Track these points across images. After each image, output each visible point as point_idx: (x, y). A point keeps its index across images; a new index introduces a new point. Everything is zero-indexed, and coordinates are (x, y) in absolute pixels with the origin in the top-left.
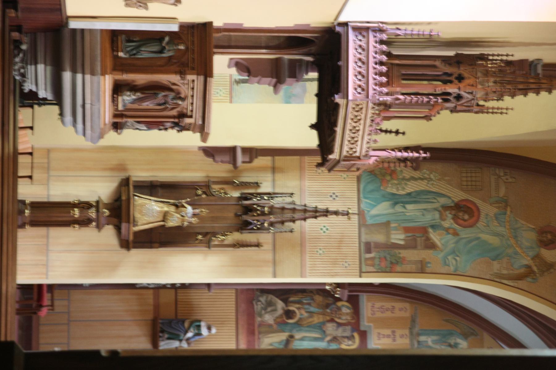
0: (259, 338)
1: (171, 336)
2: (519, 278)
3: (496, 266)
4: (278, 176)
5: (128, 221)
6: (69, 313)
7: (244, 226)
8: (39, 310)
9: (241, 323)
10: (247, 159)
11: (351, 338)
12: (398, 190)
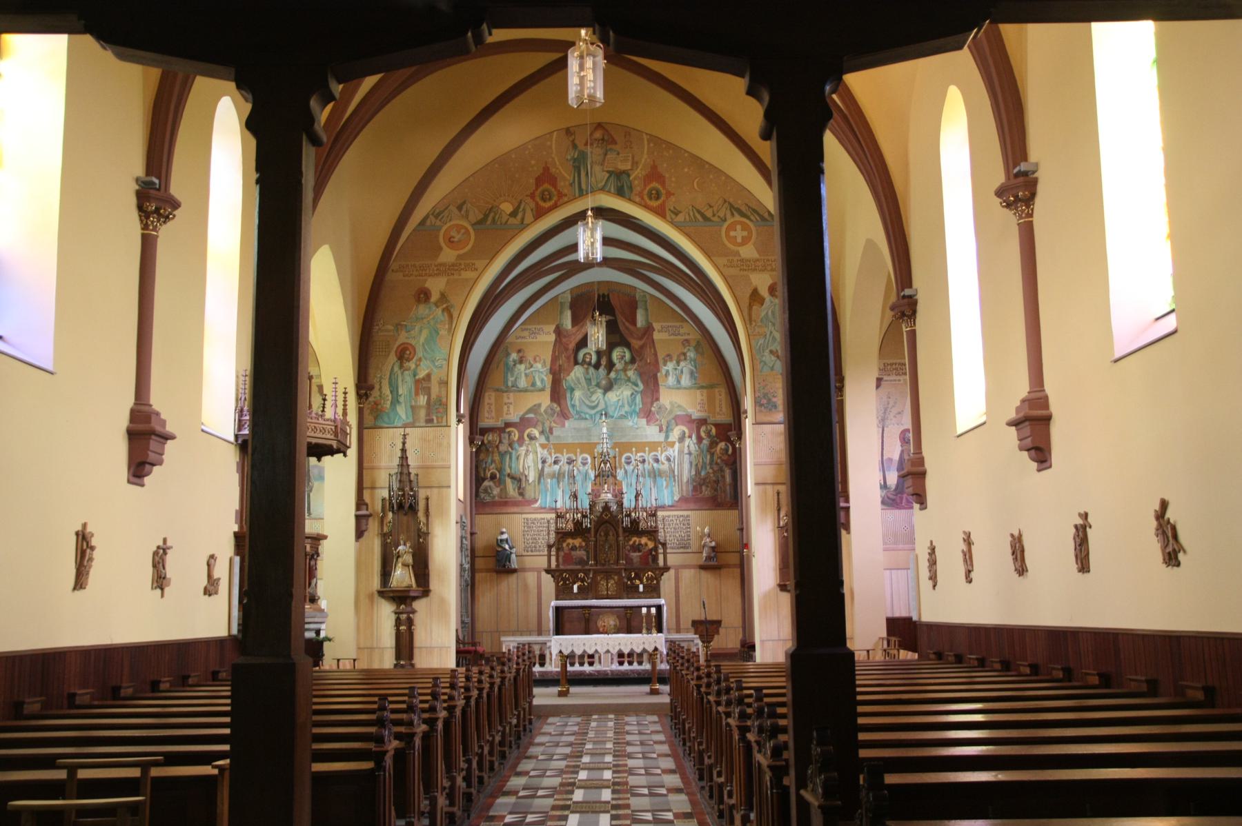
0: (510, 498)
1: (508, 560)
2: (451, 317)
3: (443, 332)
4: (378, 485)
5: (409, 591)
6: (491, 632)
7: (413, 509)
8: (479, 652)
9: (499, 511)
10: (365, 507)
11: (509, 434)
12: (388, 400)
